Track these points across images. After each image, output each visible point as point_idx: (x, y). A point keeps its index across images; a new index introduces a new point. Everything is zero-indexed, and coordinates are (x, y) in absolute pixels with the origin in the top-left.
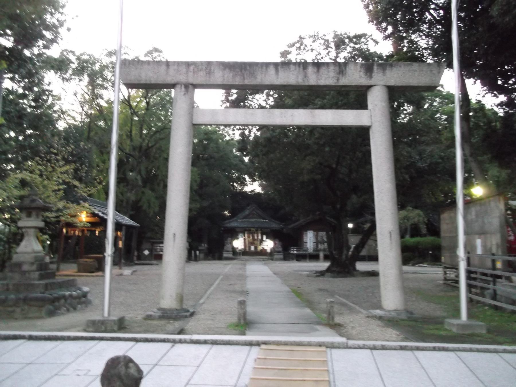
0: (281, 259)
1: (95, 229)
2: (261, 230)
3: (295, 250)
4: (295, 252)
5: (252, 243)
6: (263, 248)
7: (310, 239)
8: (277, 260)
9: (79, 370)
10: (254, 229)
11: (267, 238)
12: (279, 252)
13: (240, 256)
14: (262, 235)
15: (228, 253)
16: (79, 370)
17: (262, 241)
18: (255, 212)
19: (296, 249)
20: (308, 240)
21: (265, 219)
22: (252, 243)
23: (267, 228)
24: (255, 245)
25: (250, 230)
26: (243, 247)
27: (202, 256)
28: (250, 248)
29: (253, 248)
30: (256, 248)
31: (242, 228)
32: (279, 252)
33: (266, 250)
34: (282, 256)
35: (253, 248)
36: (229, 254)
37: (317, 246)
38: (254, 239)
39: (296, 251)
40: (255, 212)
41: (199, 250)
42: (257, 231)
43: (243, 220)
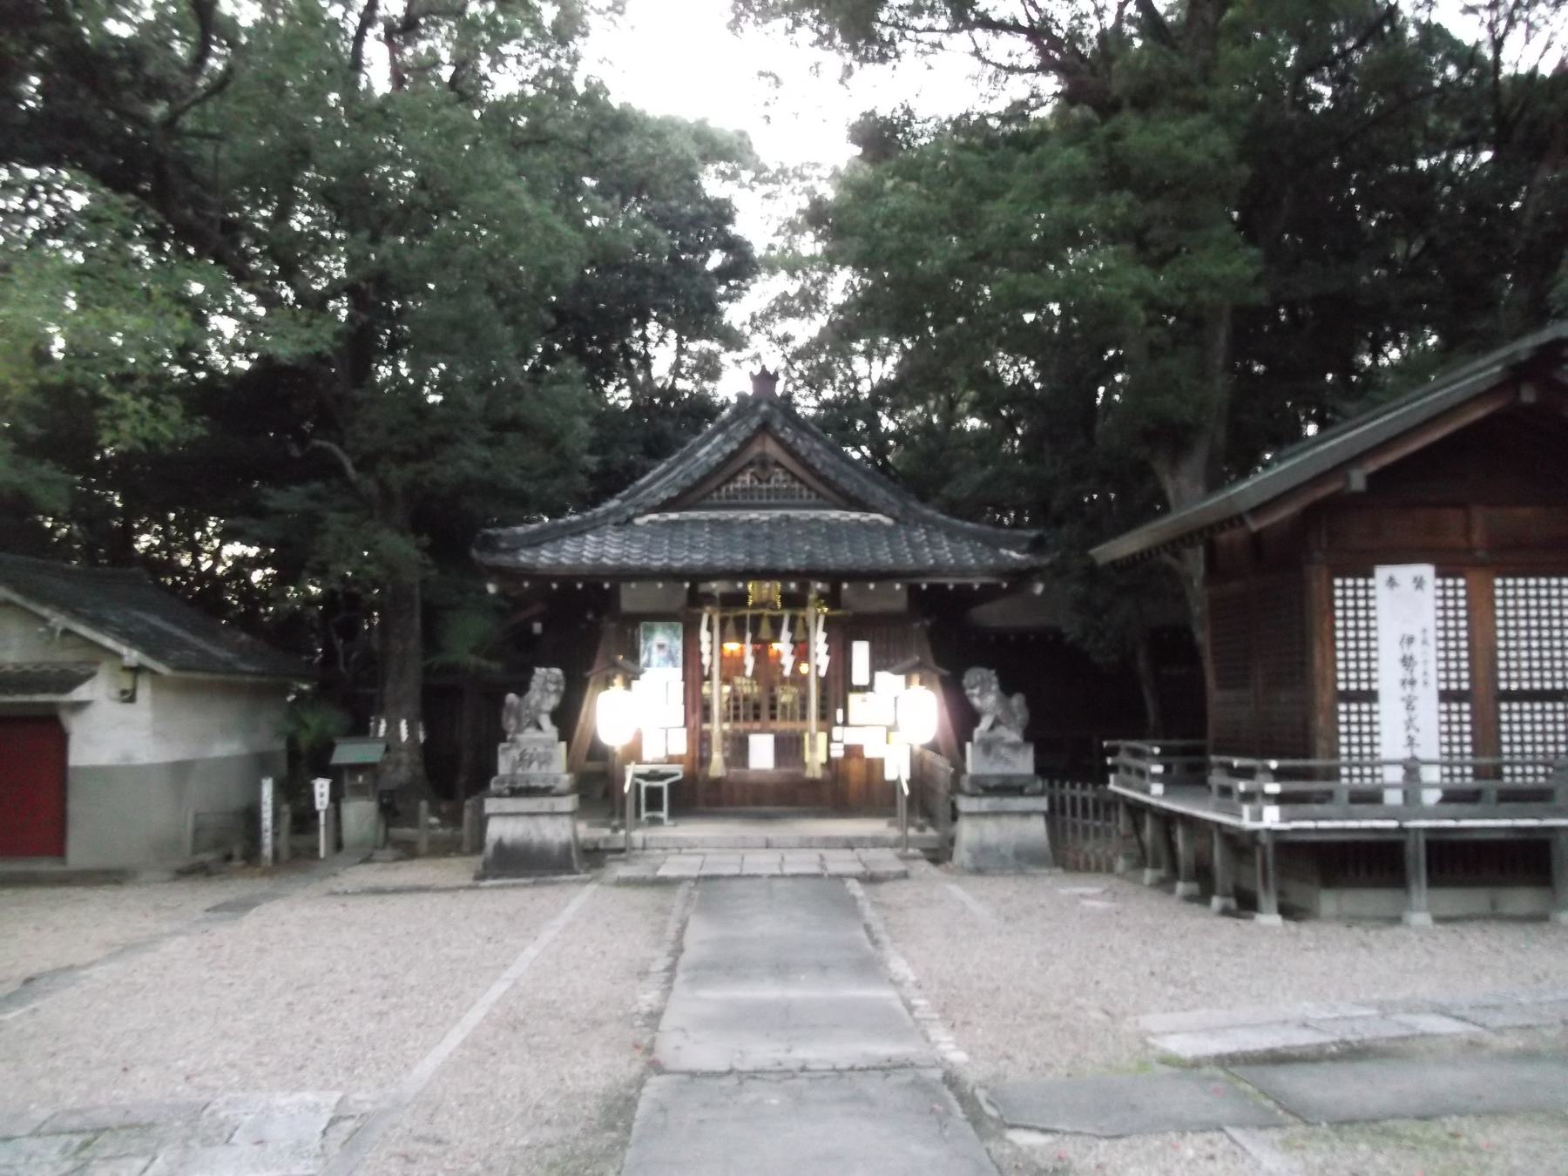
0: (1023, 860)
1: (1152, 718)
2: (832, 599)
3: (1273, 788)
4: (1272, 817)
5: (751, 711)
6: (852, 751)
7: (1407, 661)
8: (986, 864)
9: (1548, 47)
10: (770, 590)
11: (879, 662)
12: (1007, 787)
13: (655, 821)
14: (842, 635)
15: (544, 804)
16: (1548, 47)
17: (837, 688)
18: (771, 449)
19: (1278, 775)
20: (1388, 678)
21: (864, 507)
22: (751, 711)
23: (884, 576)
24: (781, 725)
25: (740, 599)
26: (679, 744)
27: (359, 815)
28: (739, 749)
29: (762, 753)
30: (789, 748)
31: (669, 575)
32: (1007, 787)
33: (875, 766)
34: (1036, 830)
35: (762, 753)
36: (553, 814)
37: (1486, 735)
38: (767, 666)
39: (1279, 799)
40: (771, 449)
41: (337, 775)
42: (793, 601)
43: (673, 516)
